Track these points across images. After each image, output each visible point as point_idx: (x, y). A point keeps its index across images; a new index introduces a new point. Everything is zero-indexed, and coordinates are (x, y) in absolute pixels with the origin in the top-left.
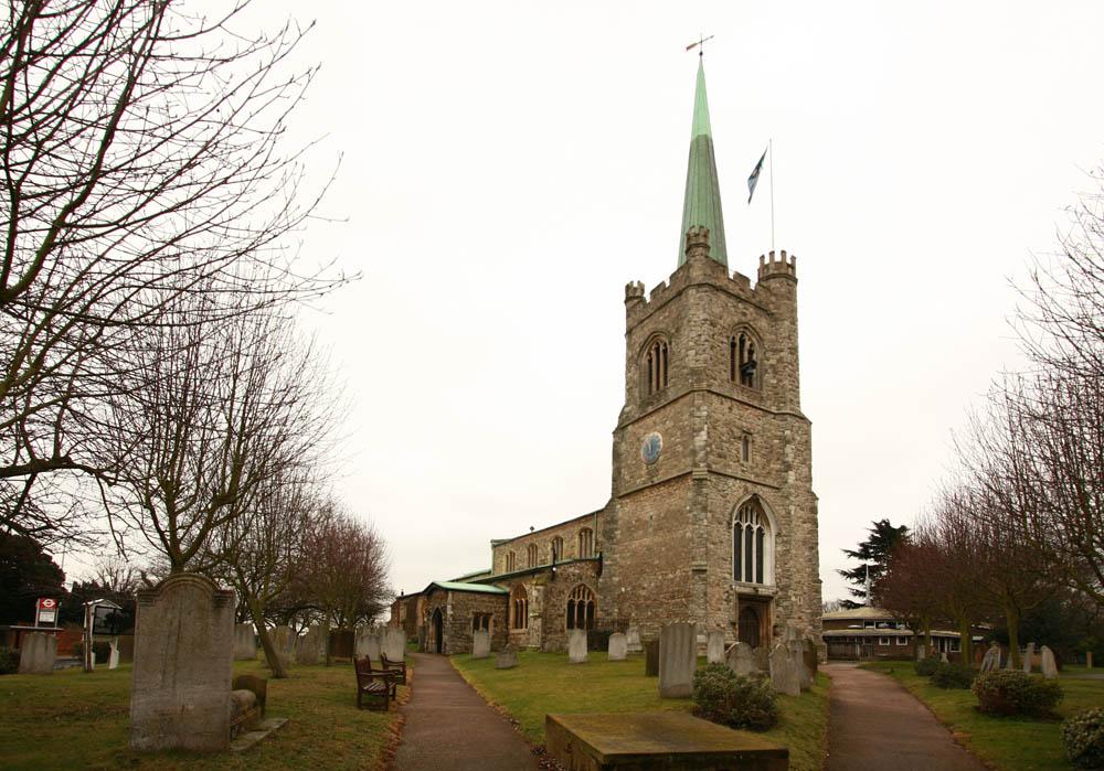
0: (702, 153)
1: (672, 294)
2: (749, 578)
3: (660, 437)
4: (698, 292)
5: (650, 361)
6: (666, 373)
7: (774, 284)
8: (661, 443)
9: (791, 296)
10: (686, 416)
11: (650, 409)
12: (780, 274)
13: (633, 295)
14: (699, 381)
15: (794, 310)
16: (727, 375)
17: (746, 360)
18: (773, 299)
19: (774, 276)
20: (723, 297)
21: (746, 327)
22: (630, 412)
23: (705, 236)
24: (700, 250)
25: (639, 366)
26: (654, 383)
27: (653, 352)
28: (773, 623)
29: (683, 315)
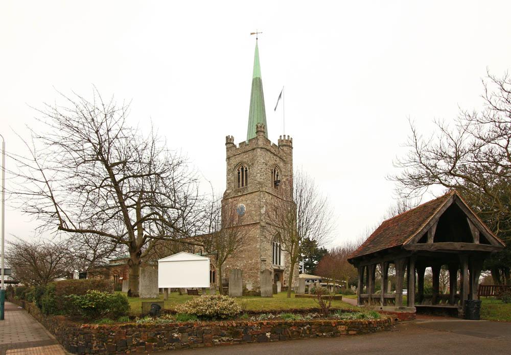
0: (257, 84)
1: (249, 147)
2: (276, 264)
3: (245, 206)
4: (261, 151)
5: (239, 173)
6: (246, 182)
7: (285, 148)
8: (245, 209)
9: (291, 154)
10: (256, 200)
11: (240, 194)
12: (286, 144)
13: (229, 141)
14: (262, 187)
15: (292, 160)
16: (270, 185)
17: (276, 180)
18: (285, 154)
19: (285, 146)
20: (269, 153)
21: (276, 166)
22: (230, 193)
23: (264, 128)
24: (262, 134)
25: (234, 174)
26: (241, 183)
27: (240, 170)
28: (284, 280)
29: (255, 158)
